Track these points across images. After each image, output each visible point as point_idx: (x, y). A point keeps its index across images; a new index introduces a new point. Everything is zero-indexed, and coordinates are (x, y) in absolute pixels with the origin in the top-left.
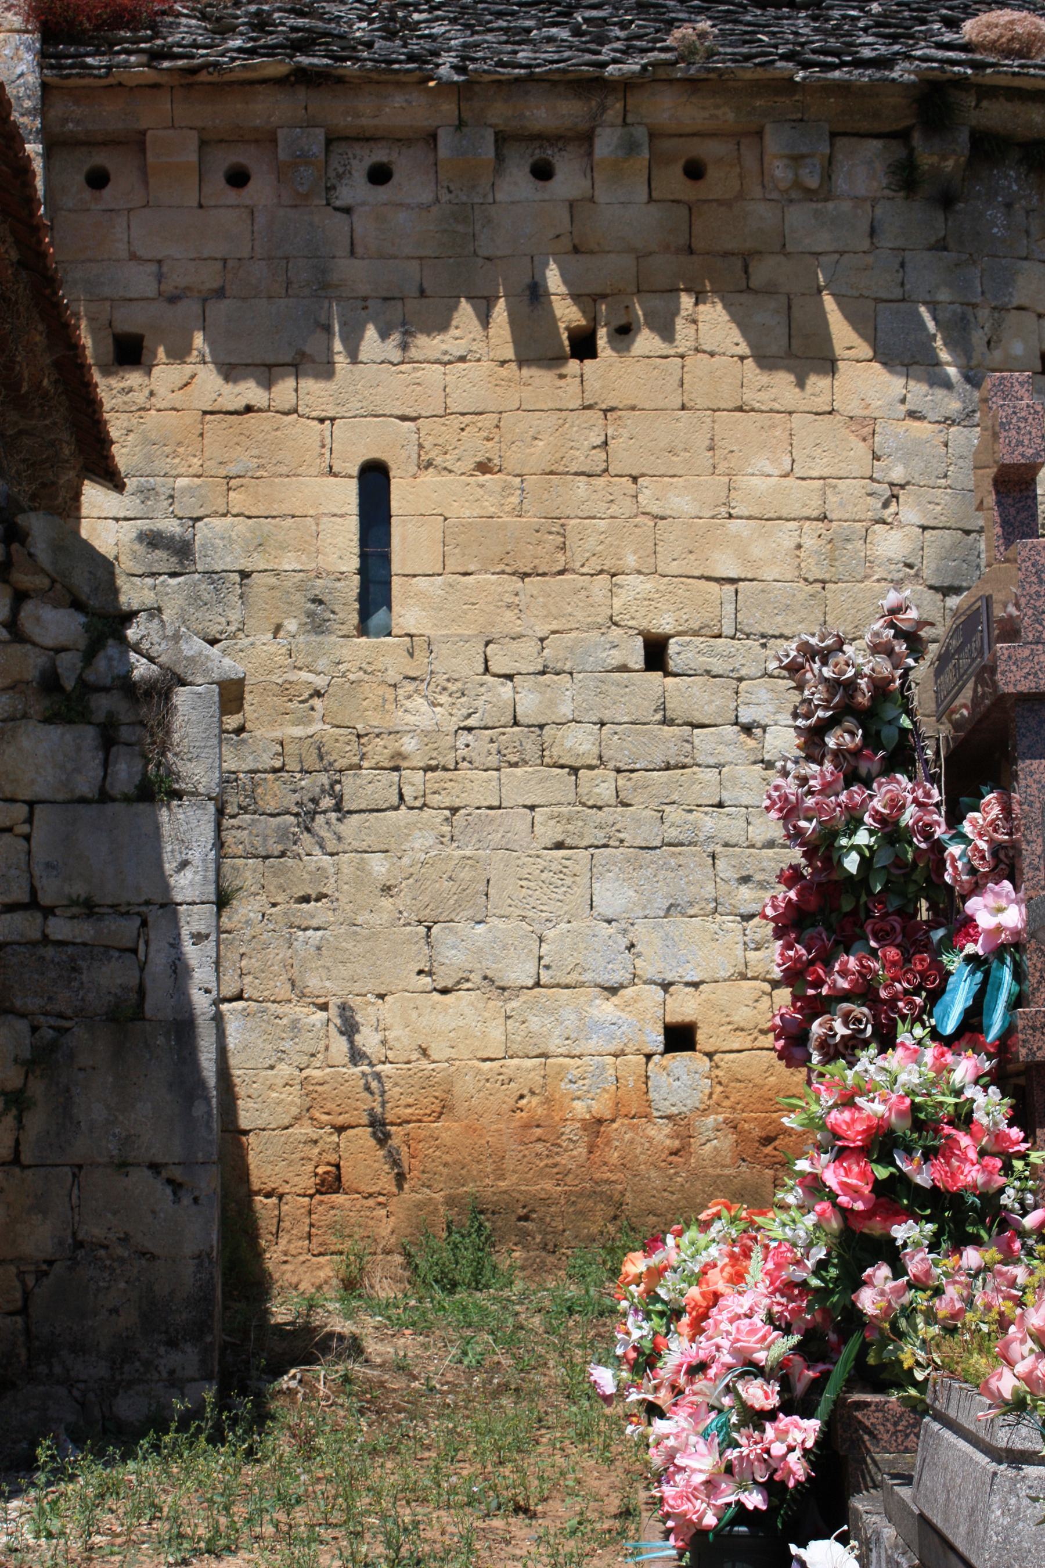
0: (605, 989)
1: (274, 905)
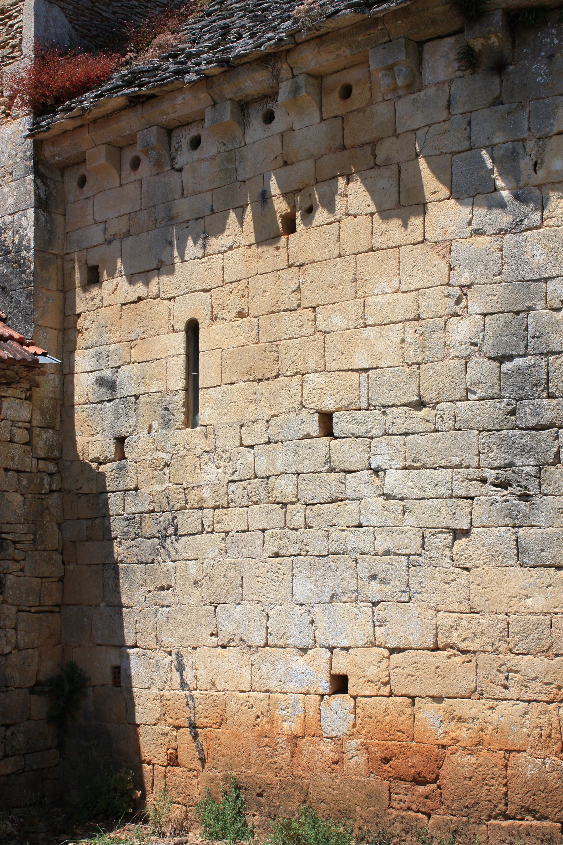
0: (301, 649)
1: (150, 592)
